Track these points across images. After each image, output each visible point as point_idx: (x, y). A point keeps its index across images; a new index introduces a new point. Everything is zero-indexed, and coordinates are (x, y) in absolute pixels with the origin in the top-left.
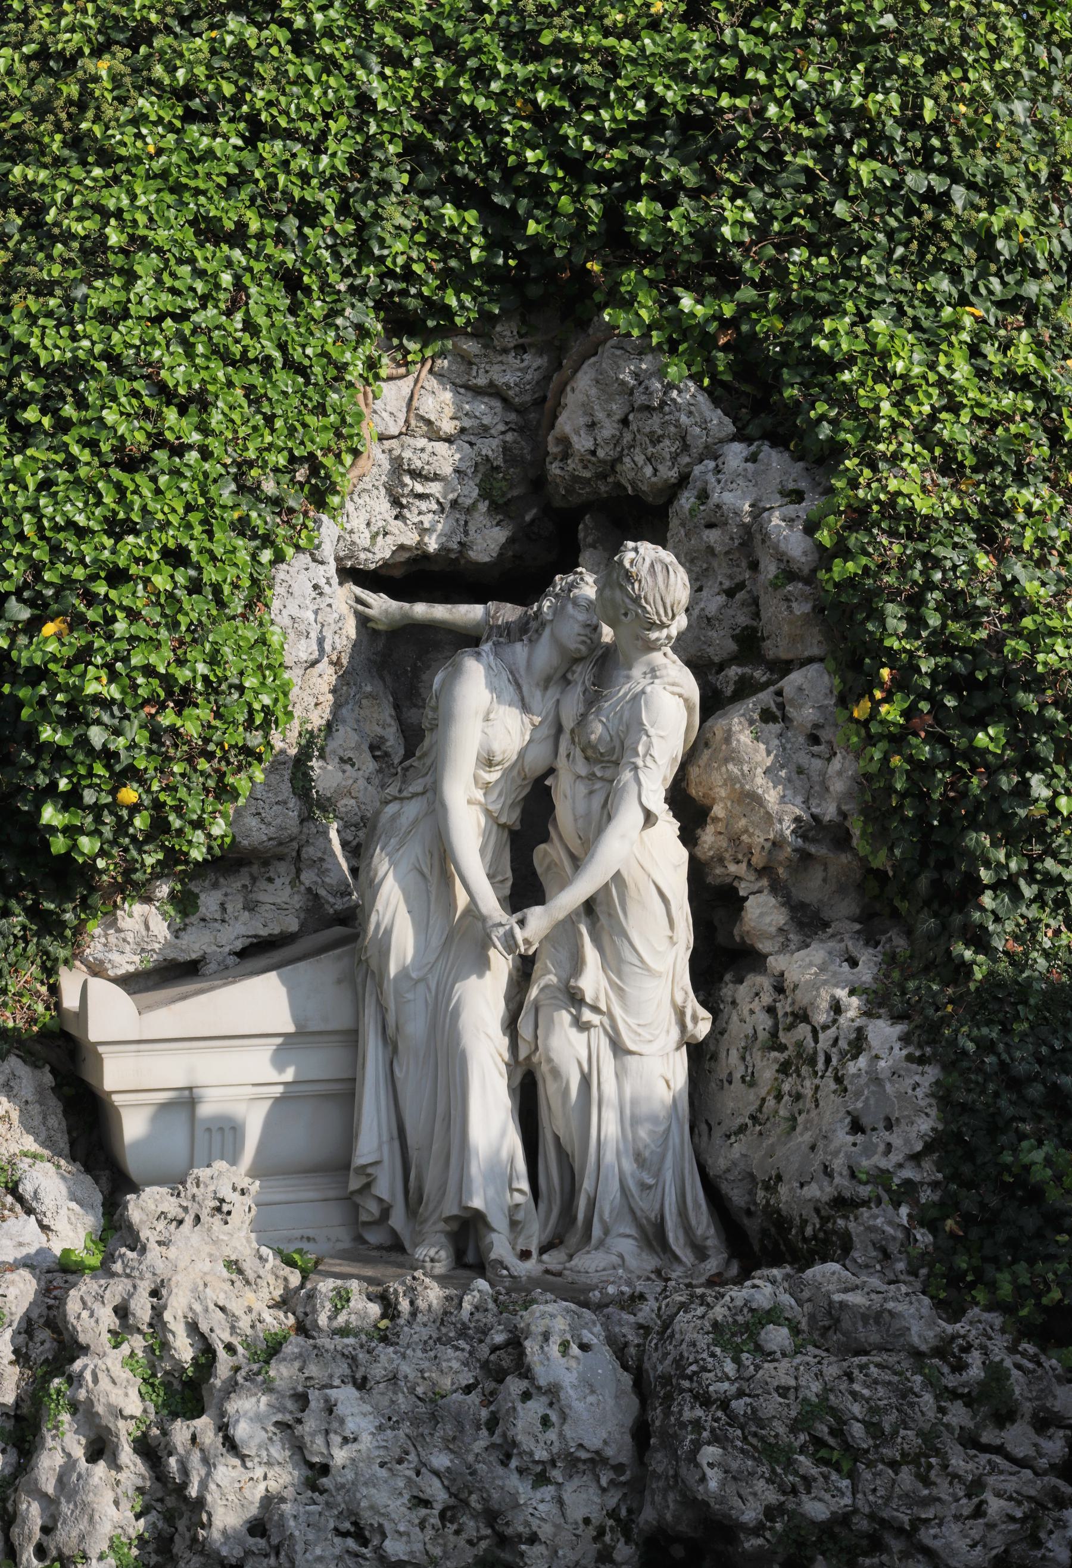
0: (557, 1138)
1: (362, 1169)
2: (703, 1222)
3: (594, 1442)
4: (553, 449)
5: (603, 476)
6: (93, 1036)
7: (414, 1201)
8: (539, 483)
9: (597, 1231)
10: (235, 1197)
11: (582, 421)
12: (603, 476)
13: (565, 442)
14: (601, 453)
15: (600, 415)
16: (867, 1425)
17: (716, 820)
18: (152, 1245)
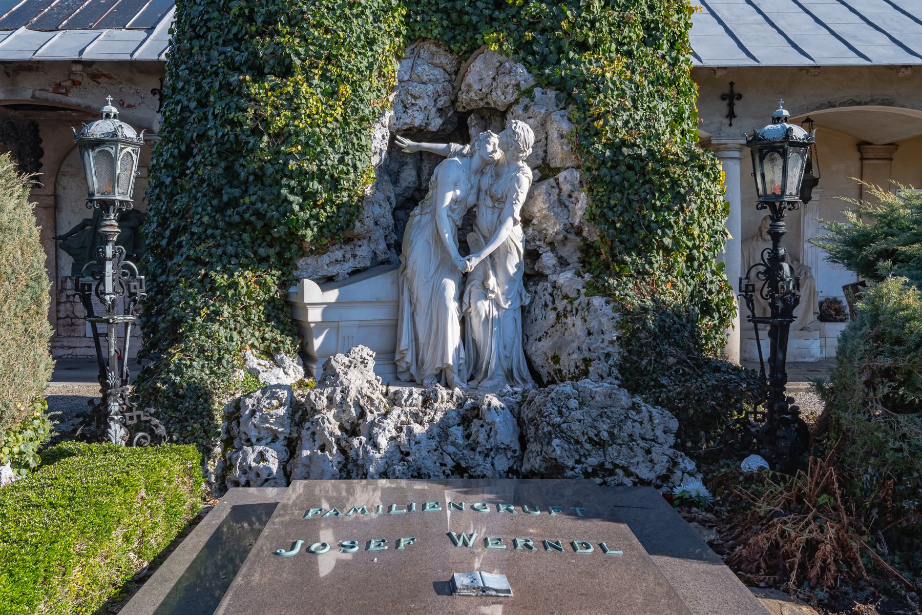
0: (474, 340)
1: (401, 352)
2: (526, 373)
3: (507, 442)
4: (463, 88)
5: (482, 99)
6: (306, 301)
7: (419, 362)
8: (454, 102)
9: (489, 373)
10: (368, 357)
11: (477, 78)
12: (482, 99)
13: (470, 86)
14: (484, 90)
15: (484, 76)
16: (609, 432)
17: (534, 225)
18: (341, 374)
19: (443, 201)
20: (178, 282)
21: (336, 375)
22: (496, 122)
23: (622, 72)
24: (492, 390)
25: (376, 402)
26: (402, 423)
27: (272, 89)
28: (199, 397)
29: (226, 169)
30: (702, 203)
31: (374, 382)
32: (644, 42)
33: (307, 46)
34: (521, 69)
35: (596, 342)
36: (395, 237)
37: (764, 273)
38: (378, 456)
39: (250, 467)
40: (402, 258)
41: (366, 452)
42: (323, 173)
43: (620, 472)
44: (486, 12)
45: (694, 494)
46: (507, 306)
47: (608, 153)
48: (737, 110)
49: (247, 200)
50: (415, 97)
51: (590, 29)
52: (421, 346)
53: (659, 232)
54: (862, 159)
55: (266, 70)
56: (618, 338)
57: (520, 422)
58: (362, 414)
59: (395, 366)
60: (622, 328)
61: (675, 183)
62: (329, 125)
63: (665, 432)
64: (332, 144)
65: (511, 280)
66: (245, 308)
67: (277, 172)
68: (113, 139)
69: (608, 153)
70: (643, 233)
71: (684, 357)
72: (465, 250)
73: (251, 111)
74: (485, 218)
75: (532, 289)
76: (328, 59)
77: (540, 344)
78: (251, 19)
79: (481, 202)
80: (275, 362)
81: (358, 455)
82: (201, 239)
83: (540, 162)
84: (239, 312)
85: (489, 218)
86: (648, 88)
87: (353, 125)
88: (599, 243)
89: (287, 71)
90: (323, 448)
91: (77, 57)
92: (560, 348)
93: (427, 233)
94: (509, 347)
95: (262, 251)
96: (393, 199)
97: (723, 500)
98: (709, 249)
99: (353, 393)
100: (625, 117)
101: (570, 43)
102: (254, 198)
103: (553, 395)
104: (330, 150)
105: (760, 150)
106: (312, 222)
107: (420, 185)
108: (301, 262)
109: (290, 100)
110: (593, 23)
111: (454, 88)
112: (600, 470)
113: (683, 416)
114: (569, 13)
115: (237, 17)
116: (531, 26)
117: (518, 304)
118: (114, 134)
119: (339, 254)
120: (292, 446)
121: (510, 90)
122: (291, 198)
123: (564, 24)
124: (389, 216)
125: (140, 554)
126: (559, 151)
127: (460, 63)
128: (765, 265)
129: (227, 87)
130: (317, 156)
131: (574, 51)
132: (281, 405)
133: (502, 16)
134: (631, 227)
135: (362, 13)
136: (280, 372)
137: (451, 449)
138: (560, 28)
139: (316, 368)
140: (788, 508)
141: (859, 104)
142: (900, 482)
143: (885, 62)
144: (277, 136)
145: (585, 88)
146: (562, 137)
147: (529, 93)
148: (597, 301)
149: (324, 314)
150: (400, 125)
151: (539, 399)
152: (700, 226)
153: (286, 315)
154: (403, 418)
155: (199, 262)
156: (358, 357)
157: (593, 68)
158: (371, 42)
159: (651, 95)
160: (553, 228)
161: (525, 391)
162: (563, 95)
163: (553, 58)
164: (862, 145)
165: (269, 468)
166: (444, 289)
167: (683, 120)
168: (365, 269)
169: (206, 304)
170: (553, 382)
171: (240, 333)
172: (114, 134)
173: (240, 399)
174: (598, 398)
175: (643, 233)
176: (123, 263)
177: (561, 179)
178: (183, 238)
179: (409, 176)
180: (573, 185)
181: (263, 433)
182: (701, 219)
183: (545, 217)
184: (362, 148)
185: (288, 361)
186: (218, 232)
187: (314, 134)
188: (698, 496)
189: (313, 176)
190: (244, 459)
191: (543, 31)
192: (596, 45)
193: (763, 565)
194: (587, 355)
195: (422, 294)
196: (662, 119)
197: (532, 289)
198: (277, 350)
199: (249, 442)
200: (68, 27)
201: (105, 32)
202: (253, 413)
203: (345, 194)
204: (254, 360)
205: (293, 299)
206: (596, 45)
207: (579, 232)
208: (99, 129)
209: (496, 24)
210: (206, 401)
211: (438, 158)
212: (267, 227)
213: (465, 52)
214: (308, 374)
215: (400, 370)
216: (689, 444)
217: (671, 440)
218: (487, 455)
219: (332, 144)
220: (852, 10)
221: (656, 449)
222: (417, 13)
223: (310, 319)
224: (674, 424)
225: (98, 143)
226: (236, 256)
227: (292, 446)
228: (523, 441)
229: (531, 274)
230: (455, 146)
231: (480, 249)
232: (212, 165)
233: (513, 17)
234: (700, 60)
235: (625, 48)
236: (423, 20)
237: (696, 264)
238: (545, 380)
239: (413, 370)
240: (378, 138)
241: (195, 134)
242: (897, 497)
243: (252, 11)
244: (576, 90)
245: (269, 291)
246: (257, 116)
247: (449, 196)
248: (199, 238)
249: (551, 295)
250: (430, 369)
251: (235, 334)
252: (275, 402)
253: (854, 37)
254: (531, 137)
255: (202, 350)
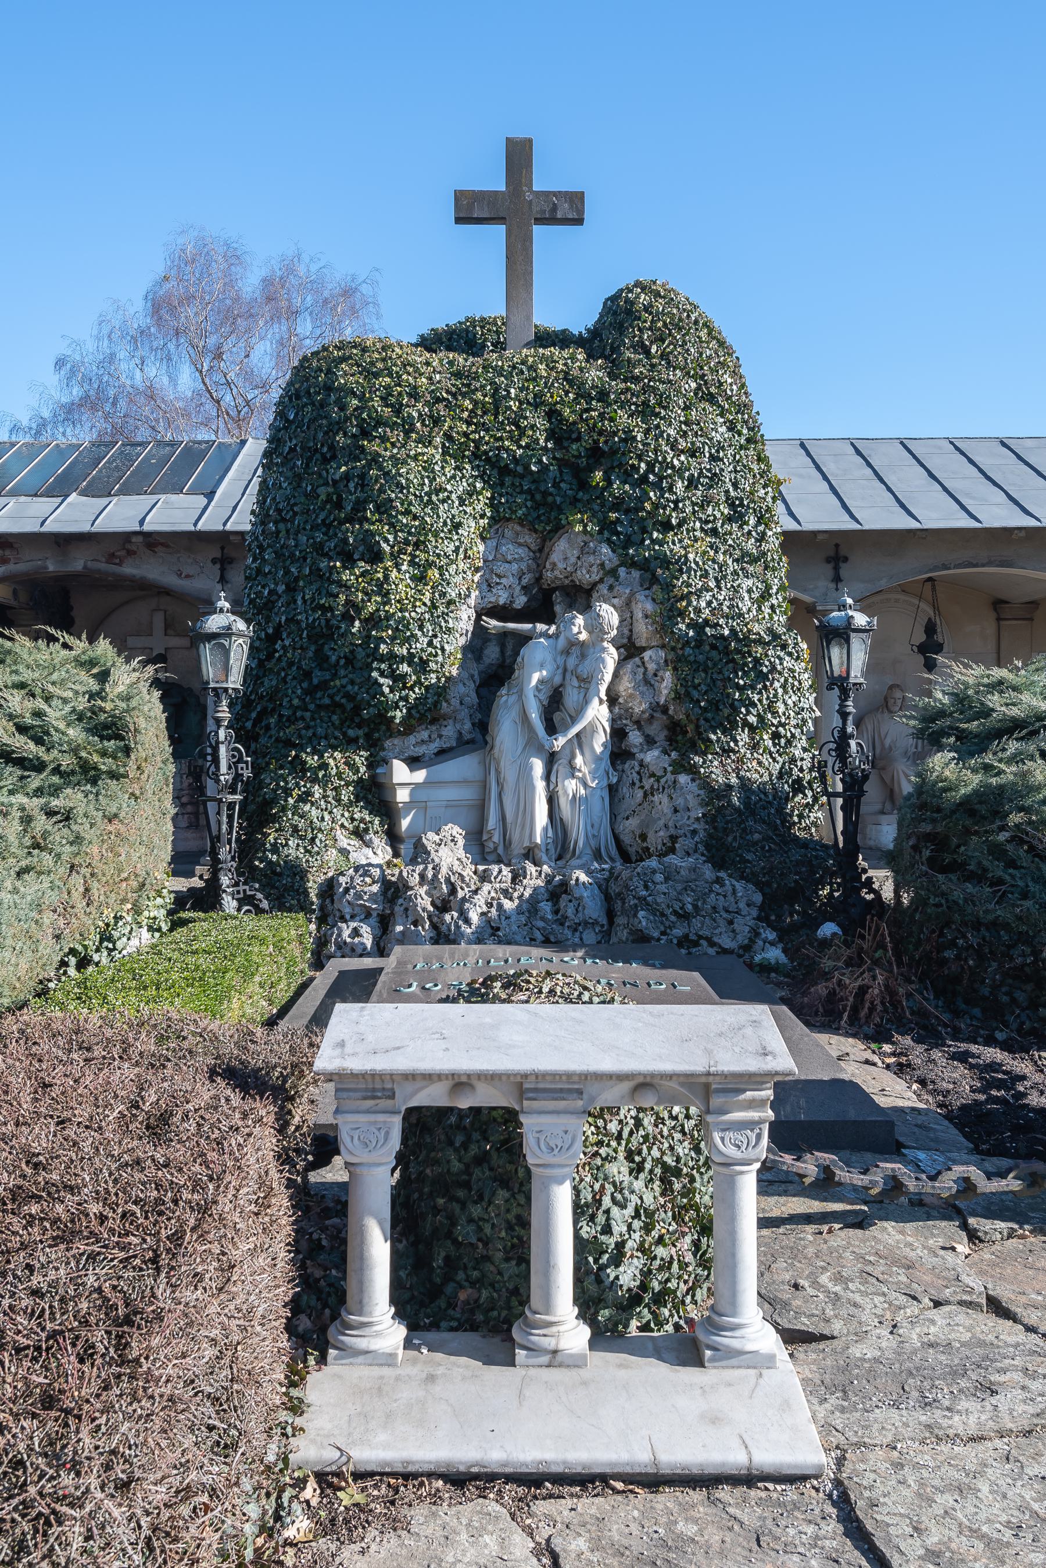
1: (489, 832)
2: (614, 851)
3: (595, 916)
4: (548, 566)
7: (507, 844)
8: (538, 579)
13: (554, 564)
19: (530, 682)
20: (268, 764)
21: (428, 853)
22: (581, 600)
23: (705, 553)
24: (579, 867)
25: (467, 879)
26: (493, 898)
27: (363, 575)
28: (295, 875)
29: (316, 652)
30: (786, 680)
31: (464, 860)
32: (729, 519)
33: (396, 532)
34: (605, 549)
35: (682, 819)
36: (479, 716)
37: (835, 750)
38: (469, 931)
39: (345, 943)
40: (488, 738)
41: (458, 927)
42: (411, 656)
43: (704, 943)
44: (569, 492)
45: (773, 962)
46: (594, 785)
47: (691, 633)
48: (843, 573)
49: (338, 683)
50: (499, 576)
51: (674, 510)
52: (509, 826)
53: (743, 710)
54: (999, 619)
55: (356, 557)
56: (704, 815)
57: (608, 898)
58: (453, 891)
59: (482, 846)
60: (707, 805)
61: (757, 661)
62: (418, 610)
63: (748, 905)
64: (421, 628)
65: (598, 759)
66: (335, 789)
67: (368, 656)
68: (227, 632)
69: (691, 633)
70: (727, 711)
71: (770, 833)
72: (552, 729)
73: (342, 598)
74: (571, 697)
75: (620, 768)
76: (417, 545)
77: (627, 823)
78: (339, 505)
79: (567, 681)
80: (364, 842)
81: (450, 930)
82: (292, 720)
83: (625, 641)
84: (329, 793)
85: (575, 698)
86: (732, 566)
87: (442, 609)
88: (685, 721)
89: (375, 557)
90: (415, 923)
91: (138, 529)
92: (647, 826)
93: (514, 713)
94: (596, 826)
95: (351, 733)
96: (476, 677)
97: (799, 964)
98: (796, 726)
99: (444, 871)
100: (708, 598)
101: (654, 524)
102: (344, 681)
103: (639, 870)
104: (419, 633)
105: (827, 636)
106: (401, 704)
107: (504, 661)
108: (388, 744)
109: (380, 585)
110: (676, 502)
111: (538, 565)
112: (684, 941)
113: (767, 890)
114: (652, 494)
115: (327, 502)
116: (616, 507)
117: (605, 783)
118: (229, 628)
119: (425, 735)
120: (384, 924)
121: (595, 569)
122: (382, 680)
123: (648, 506)
124: (474, 695)
125: (271, 1002)
126: (643, 630)
127: (544, 541)
128: (835, 742)
129: (317, 574)
130: (407, 640)
131: (658, 531)
132: (374, 882)
133: (586, 497)
134: (715, 705)
135: (448, 497)
136: (369, 852)
137: (540, 924)
138: (643, 509)
139: (405, 848)
140: (849, 963)
141: (976, 566)
142: (942, 934)
143: (997, 524)
144: (366, 621)
145: (668, 569)
146: (647, 617)
147: (613, 572)
148: (683, 779)
149: (411, 795)
150: (486, 604)
151: (625, 874)
152: (786, 704)
153: (375, 795)
154: (493, 894)
155: (289, 744)
156: (448, 835)
157: (677, 548)
158: (457, 526)
159: (735, 573)
160: (640, 707)
161: (612, 868)
162: (648, 575)
163: (636, 538)
164: (998, 604)
165: (363, 944)
166: (531, 768)
167: (770, 595)
168: (450, 749)
169: (297, 785)
170: (642, 860)
171: (330, 813)
172: (229, 628)
173: (332, 878)
174: (683, 873)
175: (727, 711)
176: (232, 746)
177: (646, 659)
178: (272, 720)
179: (492, 653)
180: (658, 664)
181: (357, 910)
182: (786, 697)
183: (631, 696)
184: (449, 630)
185: (376, 841)
186: (308, 714)
187: (404, 618)
188: (777, 963)
189: (403, 659)
190: (339, 935)
191: (627, 512)
192: (680, 525)
193: (821, 1009)
194: (672, 831)
195: (509, 774)
196: (747, 598)
197: (620, 768)
198: (366, 830)
199: (343, 919)
200: (122, 492)
201: (163, 497)
202: (347, 890)
203: (433, 676)
204: (344, 841)
205: (382, 780)
206: (680, 525)
207: (665, 710)
208: (214, 623)
209: (579, 505)
210: (302, 878)
211: (524, 639)
212: (357, 710)
213: (550, 532)
214: (396, 854)
215: (487, 850)
216: (773, 918)
217: (755, 913)
218: (576, 930)
219: (421, 628)
220: (971, 461)
221: (739, 921)
222: (501, 495)
223: (398, 800)
224: (758, 898)
225: (214, 636)
226: (326, 738)
227: (384, 924)
228: (610, 915)
229: (619, 752)
230: (541, 627)
231: (567, 728)
232: (301, 648)
233: (597, 498)
234: (799, 523)
235: (710, 526)
236: (507, 501)
237: (783, 741)
238: (634, 858)
239: (500, 850)
240: (464, 619)
241: (284, 618)
242: (940, 948)
243: (340, 497)
244: (659, 571)
245: (358, 771)
246: (348, 602)
247: (536, 677)
248: (288, 720)
249: (638, 773)
250: (517, 849)
251: (327, 817)
252: (368, 880)
253: (967, 495)
254: (615, 619)
255: (296, 830)
